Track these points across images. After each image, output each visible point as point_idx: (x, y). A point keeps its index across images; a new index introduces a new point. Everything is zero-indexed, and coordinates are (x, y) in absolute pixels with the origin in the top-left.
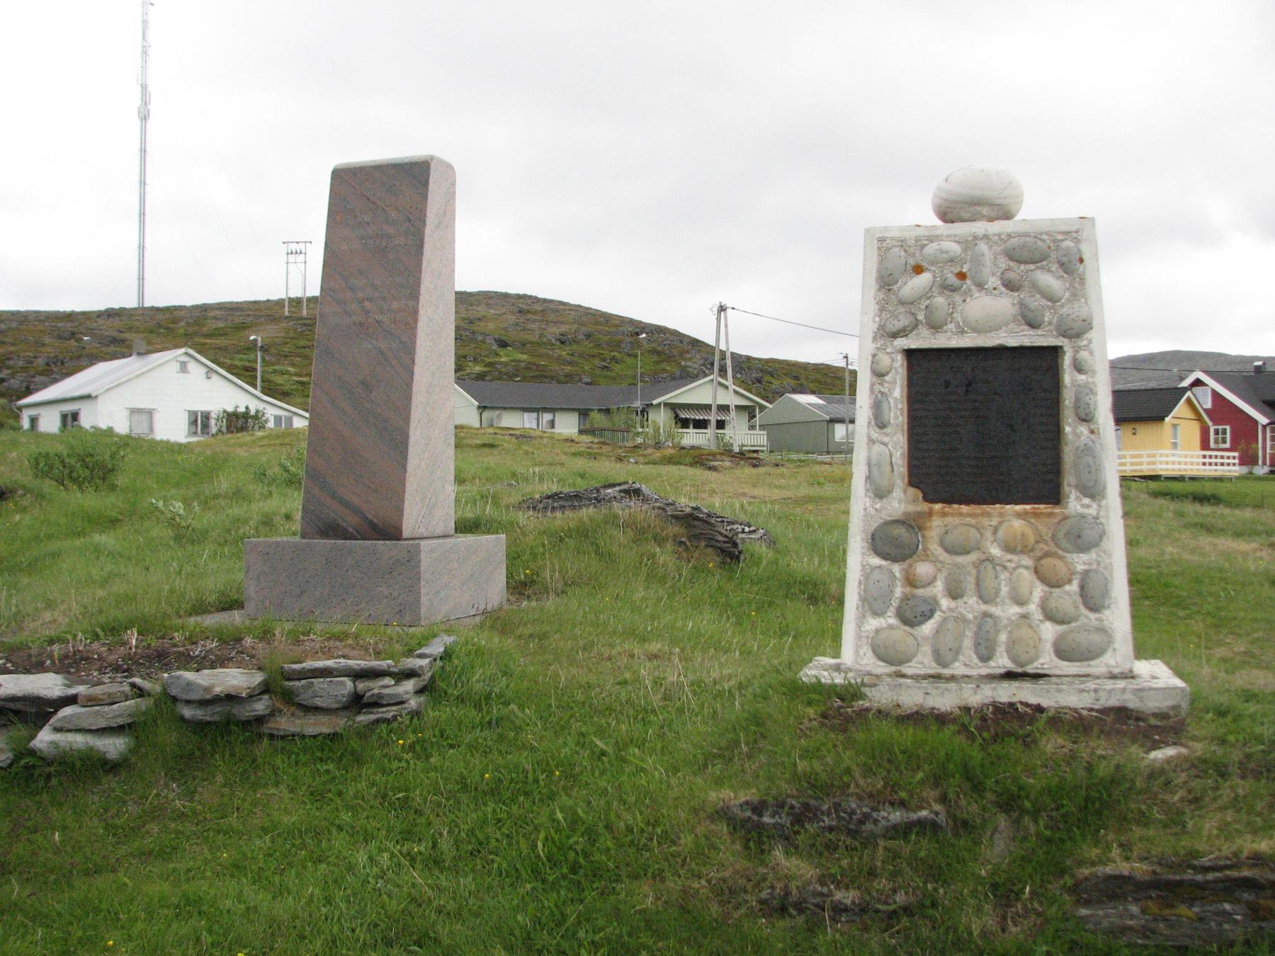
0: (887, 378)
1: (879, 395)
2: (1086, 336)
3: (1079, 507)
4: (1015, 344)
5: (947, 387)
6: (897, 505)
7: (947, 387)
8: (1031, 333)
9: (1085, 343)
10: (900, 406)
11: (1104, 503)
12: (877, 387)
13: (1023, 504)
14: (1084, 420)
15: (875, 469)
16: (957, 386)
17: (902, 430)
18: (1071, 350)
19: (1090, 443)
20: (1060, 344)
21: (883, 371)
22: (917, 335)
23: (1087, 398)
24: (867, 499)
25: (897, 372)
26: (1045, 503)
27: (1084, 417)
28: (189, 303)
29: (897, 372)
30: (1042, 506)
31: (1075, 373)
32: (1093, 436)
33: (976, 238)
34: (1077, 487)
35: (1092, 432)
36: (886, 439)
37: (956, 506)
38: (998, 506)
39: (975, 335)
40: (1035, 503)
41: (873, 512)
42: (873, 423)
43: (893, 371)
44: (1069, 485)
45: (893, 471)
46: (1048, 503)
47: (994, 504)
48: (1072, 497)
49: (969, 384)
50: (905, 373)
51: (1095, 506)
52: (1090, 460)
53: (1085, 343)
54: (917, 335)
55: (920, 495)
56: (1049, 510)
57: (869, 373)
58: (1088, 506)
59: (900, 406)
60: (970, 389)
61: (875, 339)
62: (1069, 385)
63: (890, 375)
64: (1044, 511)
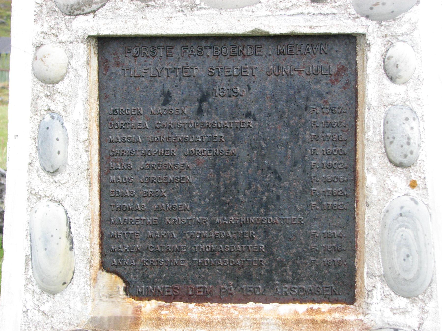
0: (60, 86)
1: (48, 118)
2: (407, 16)
3: (388, 313)
4: (284, 30)
5: (166, 102)
6: (79, 305)
7: (166, 102)
8: (312, 10)
9: (405, 28)
10: (84, 136)
11: (431, 306)
12: (44, 103)
13: (294, 300)
14: (400, 165)
15: (39, 245)
16: (183, 101)
17: (89, 177)
18: (380, 41)
19: (409, 205)
20: (361, 31)
21: (52, 74)
22: (113, 10)
23: (407, 127)
24: (29, 296)
25: (78, 76)
26: (329, 301)
27: (399, 159)
28: (10, 63)
29: (78, 76)
30: (325, 307)
31: (386, 81)
32: (413, 192)
33: (248, 308)
34: (385, 278)
35: (413, 185)
36: (59, 194)
37: (180, 305)
38: (251, 304)
39: (212, 11)
40: (314, 301)
41: (39, 317)
42: (37, 164)
43: (71, 74)
44: (371, 275)
45: (72, 249)
46: (336, 301)
47: (245, 301)
48: (377, 294)
49: (203, 99)
50: (94, 77)
51: (415, 310)
52: (409, 233)
53: (405, 28)
54: (113, 10)
55: (121, 285)
56: (338, 316)
57: (29, 77)
58: (404, 312)
59: (84, 136)
60: (205, 105)
61: (38, 15)
62: (374, 103)
63: (66, 80)
64: (329, 318)
